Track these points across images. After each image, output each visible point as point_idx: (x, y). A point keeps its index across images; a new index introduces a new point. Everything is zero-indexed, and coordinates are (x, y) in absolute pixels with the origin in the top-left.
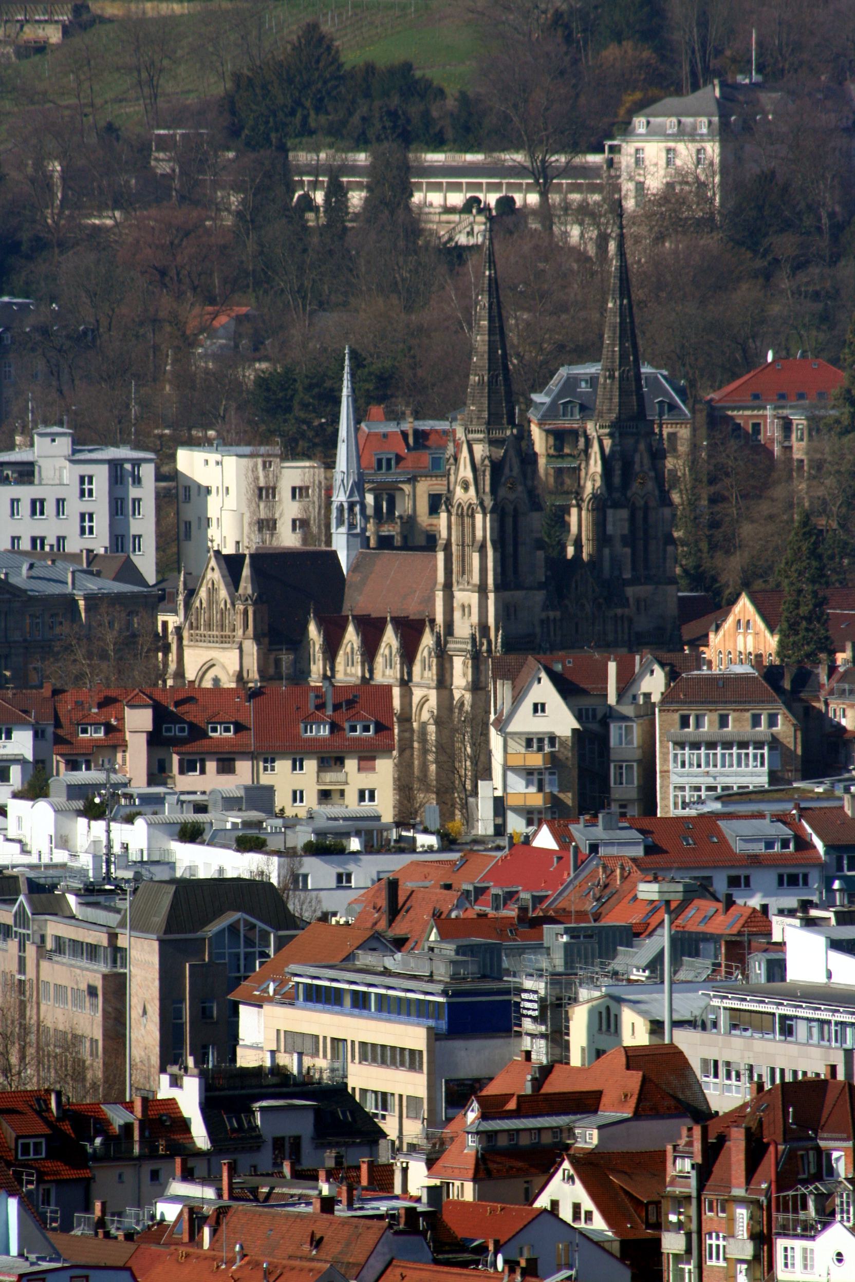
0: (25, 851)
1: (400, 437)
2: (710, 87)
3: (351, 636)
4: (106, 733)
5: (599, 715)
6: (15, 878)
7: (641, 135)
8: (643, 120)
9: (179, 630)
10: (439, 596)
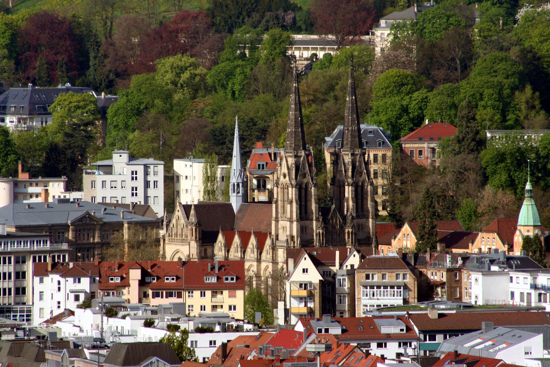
0: (81, 330)
1: (268, 155)
2: (413, 7)
3: (237, 240)
4: (121, 280)
5: (332, 274)
6: (68, 342)
7: (383, 28)
8: (384, 21)
9: (164, 236)
10: (273, 223)
